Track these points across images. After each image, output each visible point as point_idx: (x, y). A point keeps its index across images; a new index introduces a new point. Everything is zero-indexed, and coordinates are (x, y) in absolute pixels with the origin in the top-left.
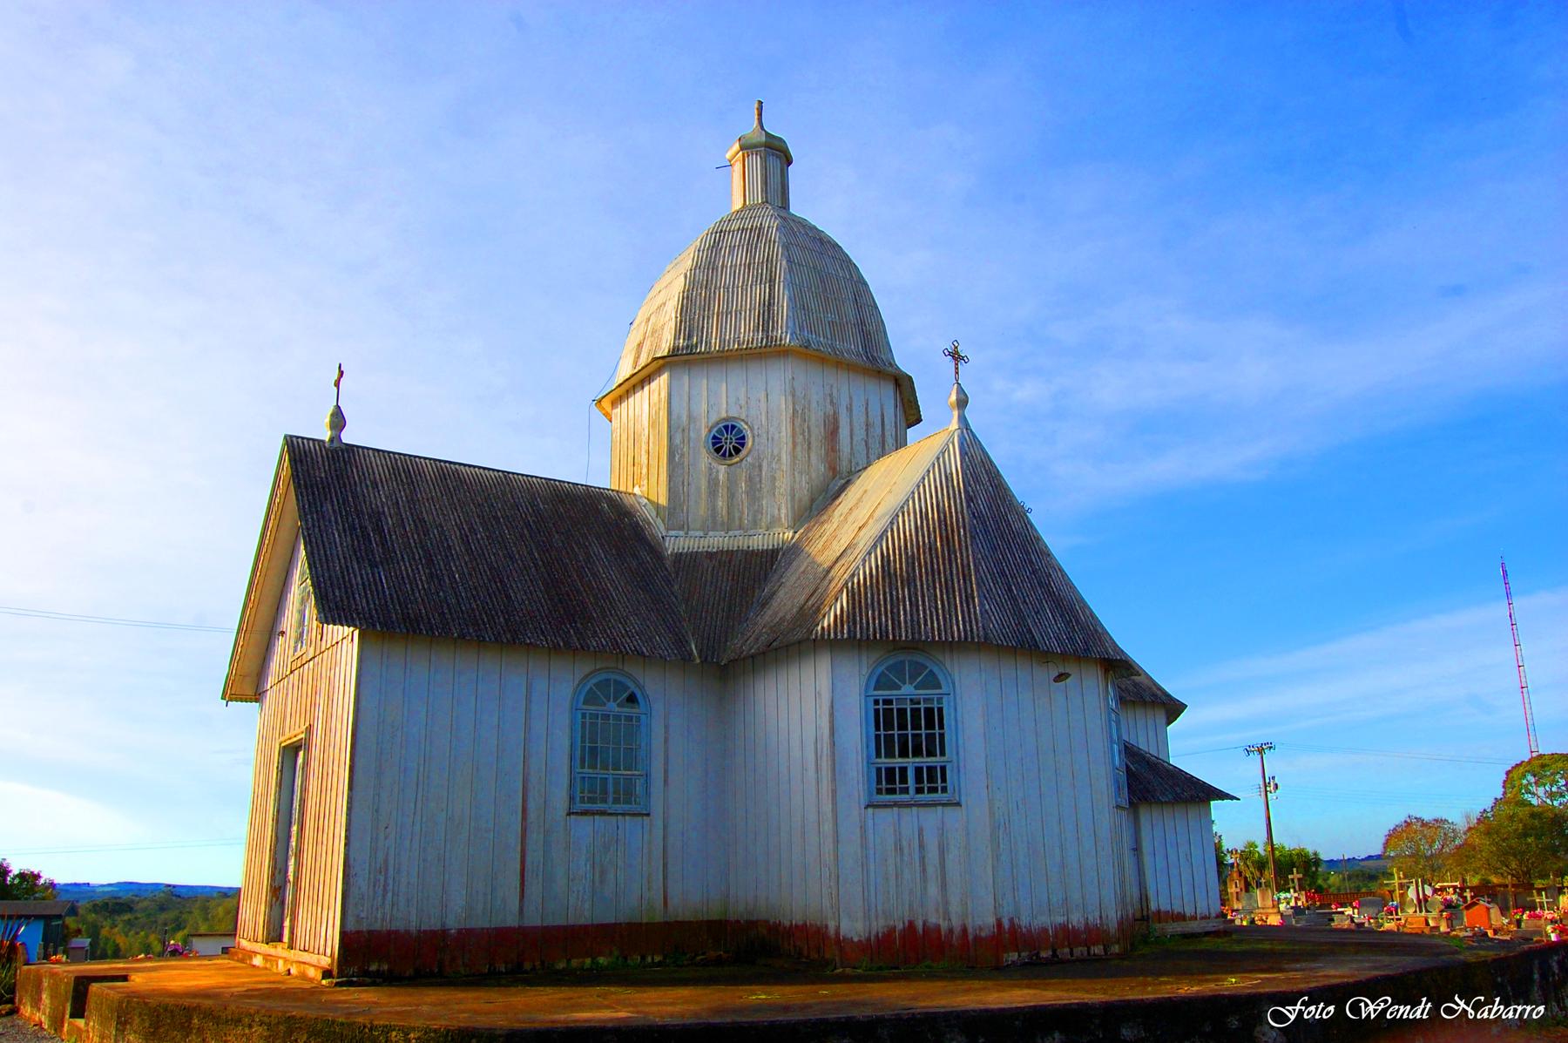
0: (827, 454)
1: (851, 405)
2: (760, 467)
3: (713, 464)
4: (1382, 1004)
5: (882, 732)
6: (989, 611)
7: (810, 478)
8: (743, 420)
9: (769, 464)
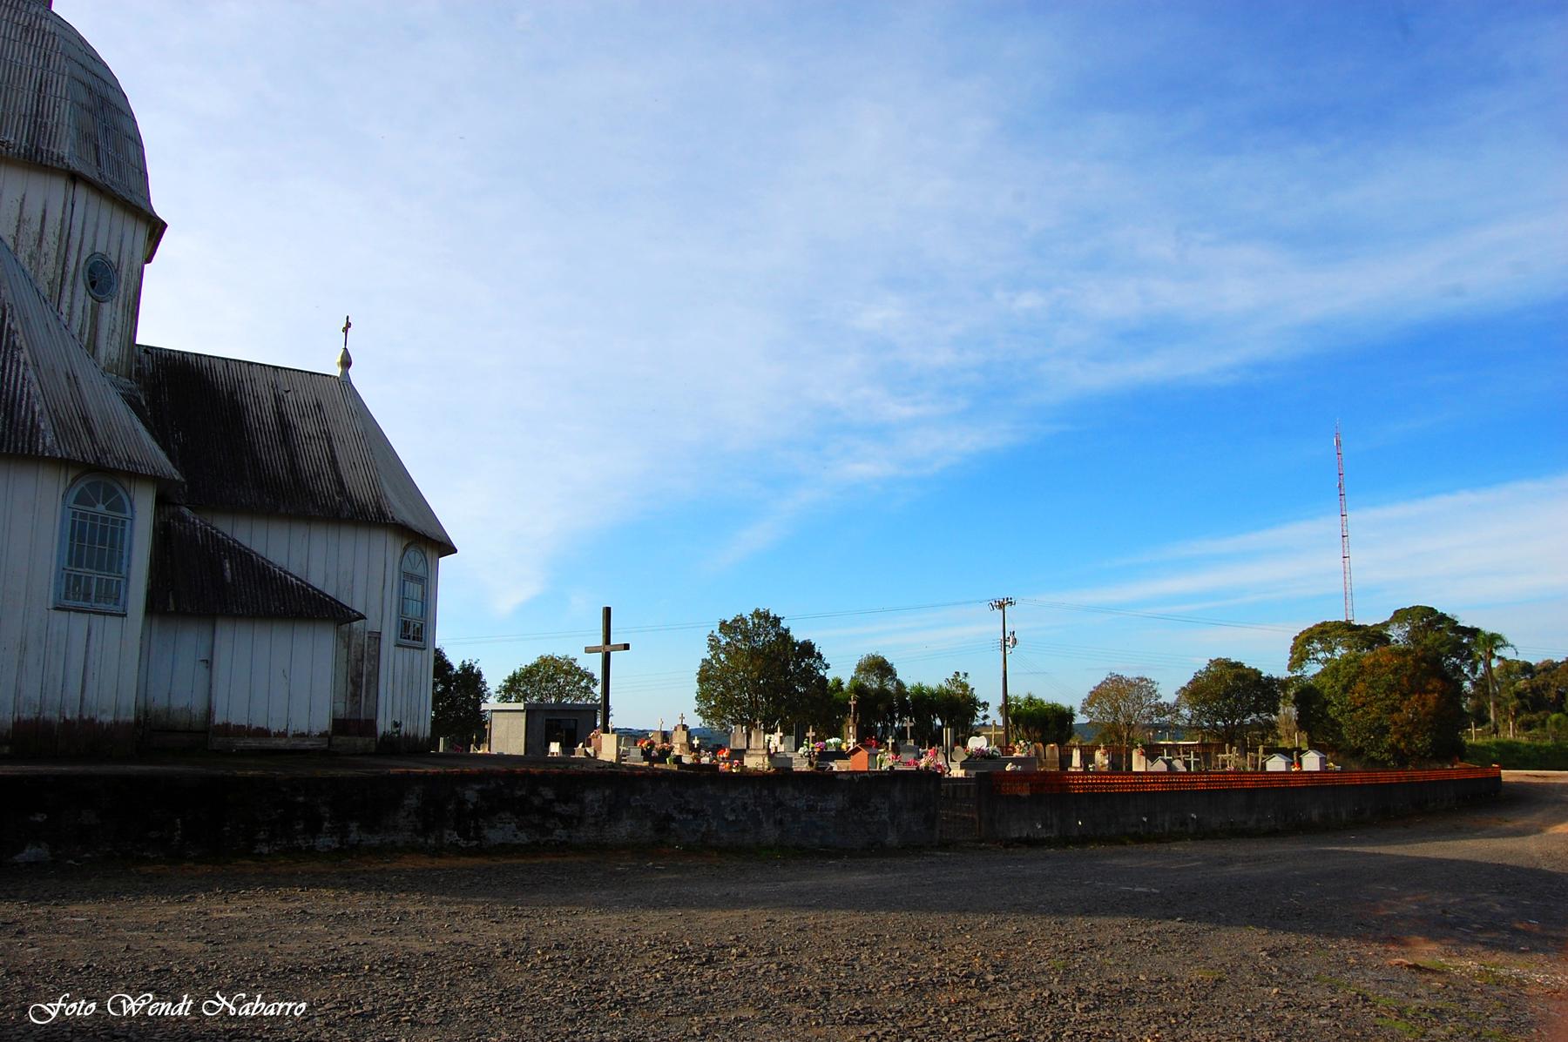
4: (144, 1001)
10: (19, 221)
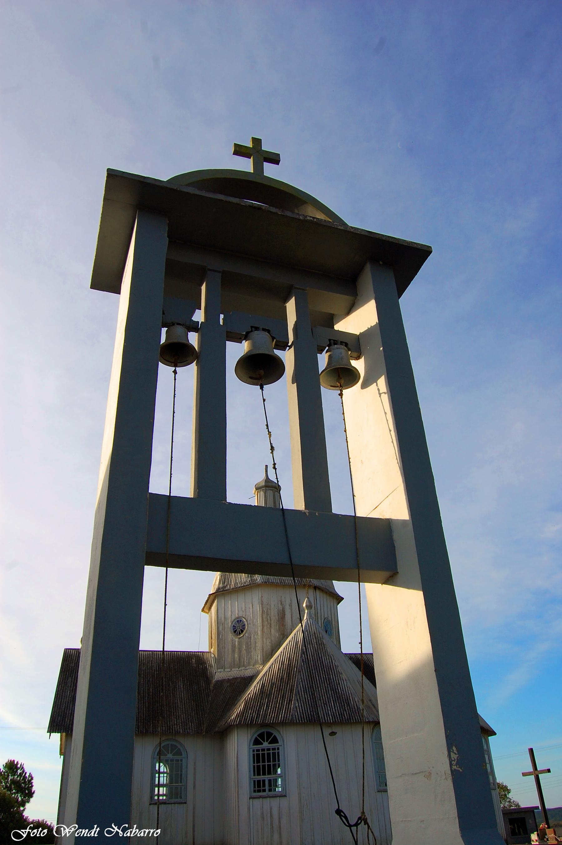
1: (291, 604)
2: (251, 637)
5: (256, 764)
6: (298, 707)
7: (272, 641)
8: (244, 618)
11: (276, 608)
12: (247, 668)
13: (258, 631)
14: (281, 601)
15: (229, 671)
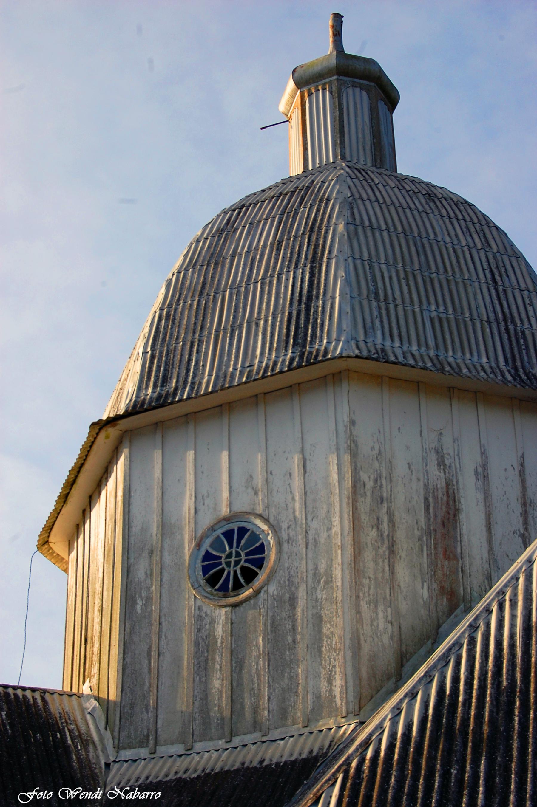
0: (433, 564)
3: (204, 609)
4: (77, 791)
7: (397, 614)
8: (260, 516)
9: (311, 591)
10: (524, 504)
11: (418, 479)
12: (275, 734)
13: (330, 567)
14: (439, 451)
15: (180, 756)
